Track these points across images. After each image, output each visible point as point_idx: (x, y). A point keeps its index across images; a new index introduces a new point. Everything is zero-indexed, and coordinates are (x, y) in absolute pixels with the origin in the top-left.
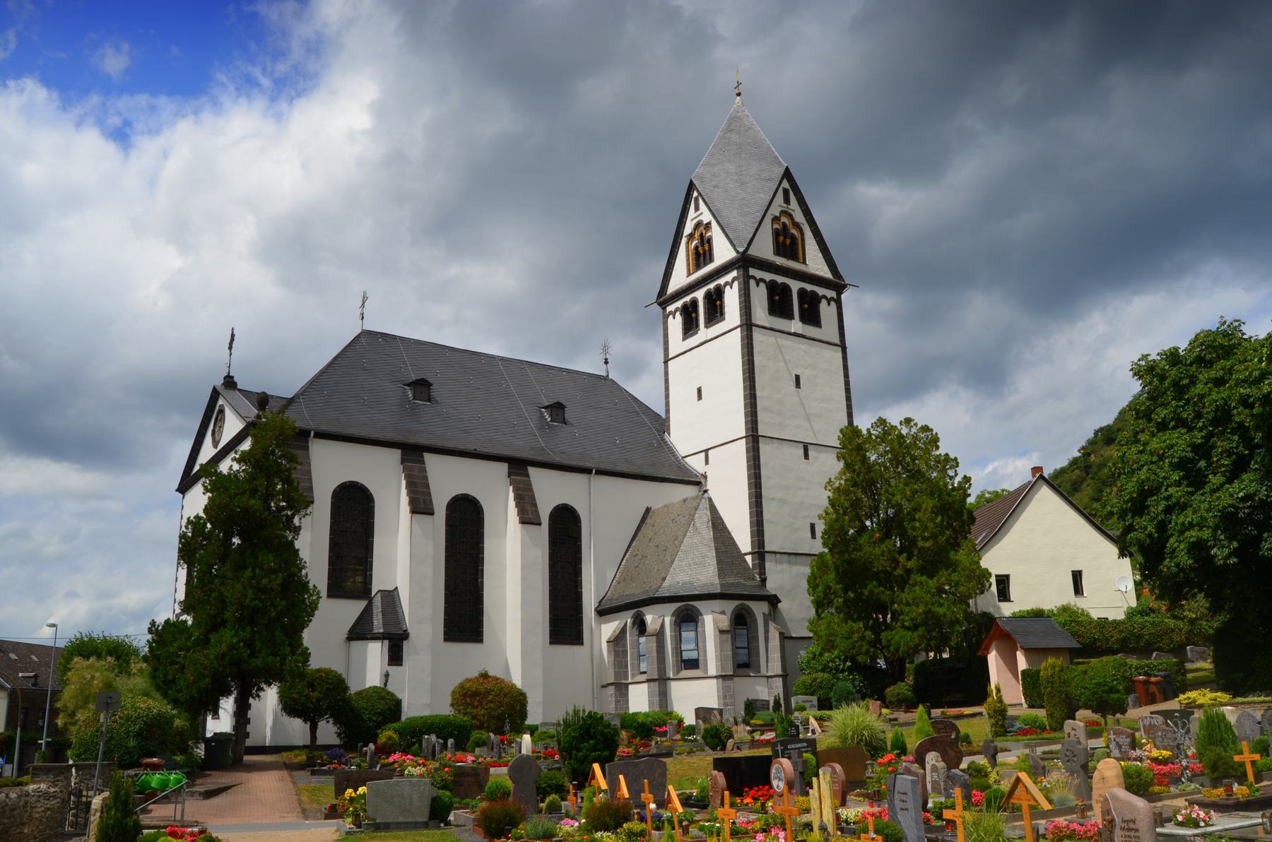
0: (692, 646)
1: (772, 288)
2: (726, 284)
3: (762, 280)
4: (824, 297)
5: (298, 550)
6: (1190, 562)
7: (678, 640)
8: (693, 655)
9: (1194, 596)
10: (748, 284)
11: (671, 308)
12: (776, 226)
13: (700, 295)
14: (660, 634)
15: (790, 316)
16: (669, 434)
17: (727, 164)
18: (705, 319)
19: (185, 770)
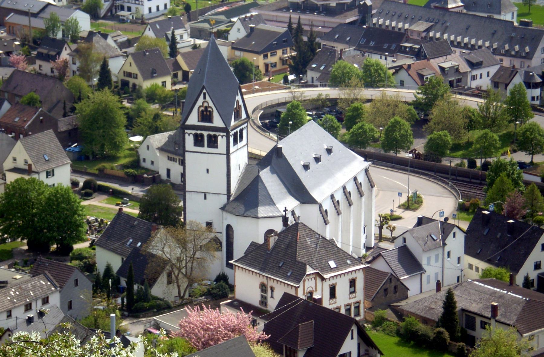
1: (196, 136)
12: (202, 108)
15: (203, 146)
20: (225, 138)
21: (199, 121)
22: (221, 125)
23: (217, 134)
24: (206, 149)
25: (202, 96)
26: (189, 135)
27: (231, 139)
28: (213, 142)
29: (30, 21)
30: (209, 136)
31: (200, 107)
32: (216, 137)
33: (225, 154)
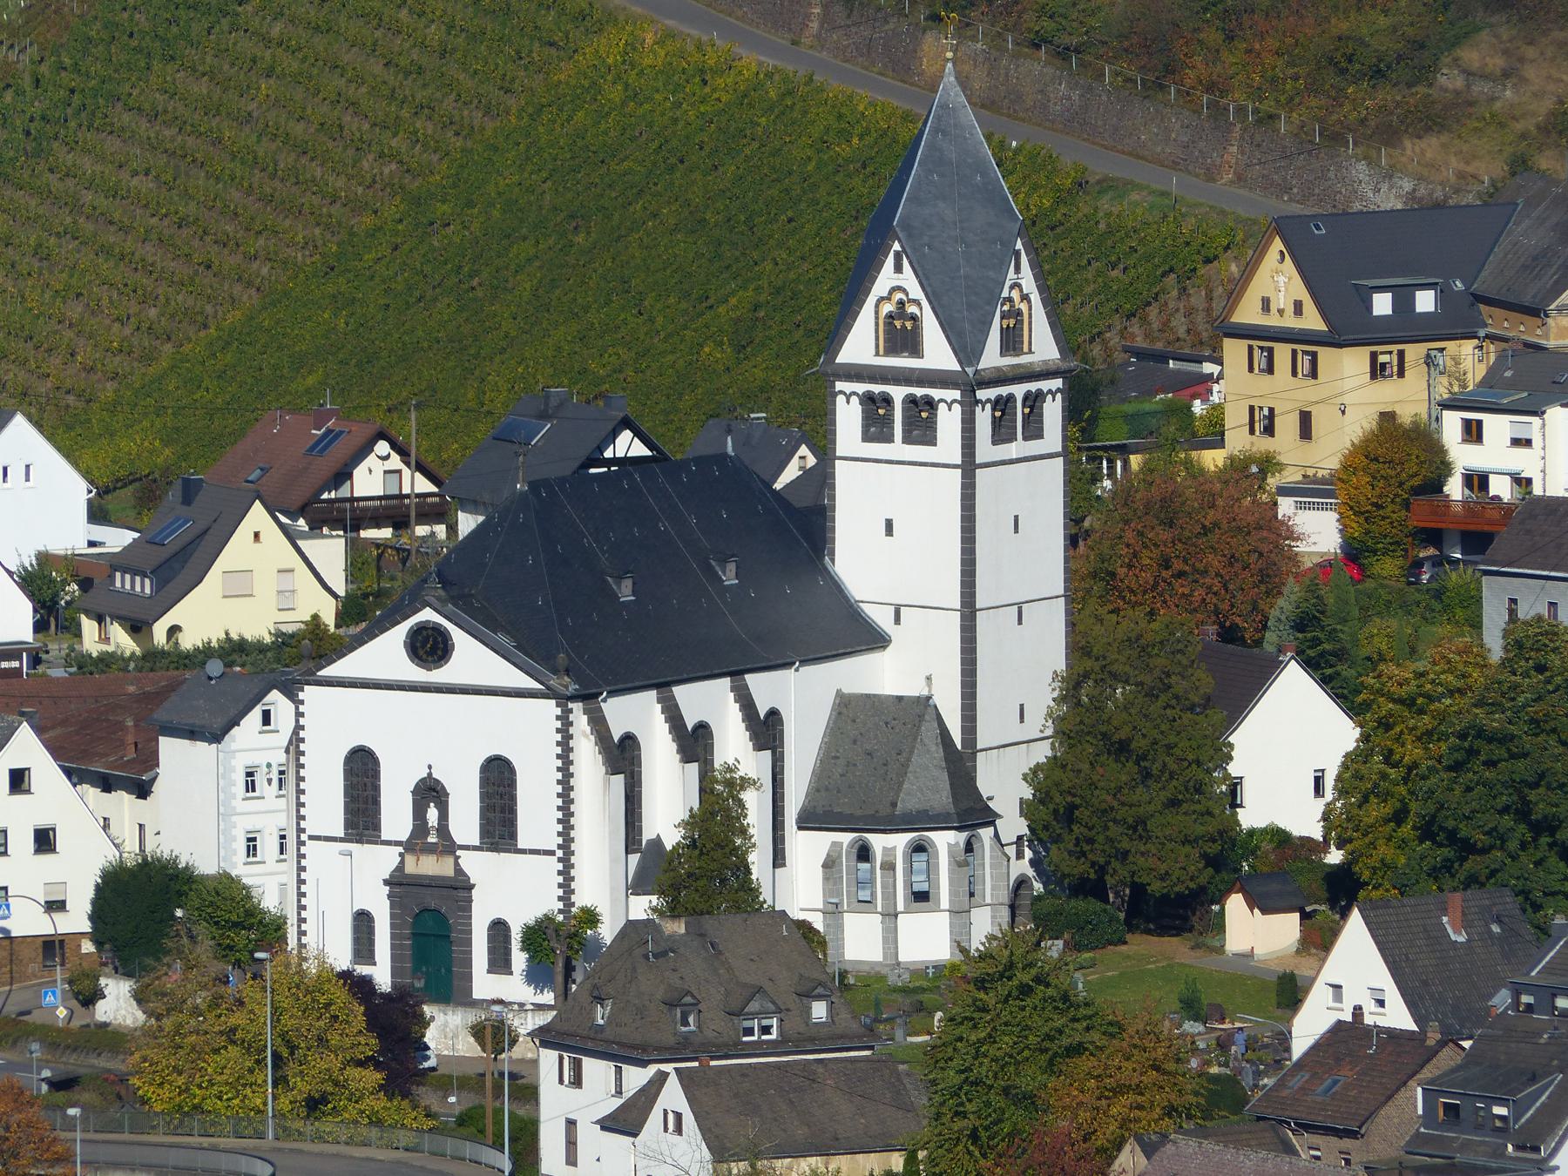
0: (923, 877)
1: (869, 400)
2: (1050, 391)
3: (854, 393)
4: (942, 400)
5: (239, 725)
6: (641, 907)
7: (909, 871)
8: (924, 887)
9: (420, 979)
10: (973, 413)
11: (982, 394)
12: (887, 308)
13: (1019, 390)
14: (889, 867)
15: (889, 439)
16: (833, 561)
17: (941, 204)
18: (904, 431)
19: (1236, 889)
20: (957, 408)
21: (877, 354)
22: (951, 364)
23: (936, 393)
24: (897, 448)
27: (984, 418)
28: (921, 425)
29: (523, 852)
30: (911, 401)
31: (881, 300)
32: (930, 404)
33: (955, 466)
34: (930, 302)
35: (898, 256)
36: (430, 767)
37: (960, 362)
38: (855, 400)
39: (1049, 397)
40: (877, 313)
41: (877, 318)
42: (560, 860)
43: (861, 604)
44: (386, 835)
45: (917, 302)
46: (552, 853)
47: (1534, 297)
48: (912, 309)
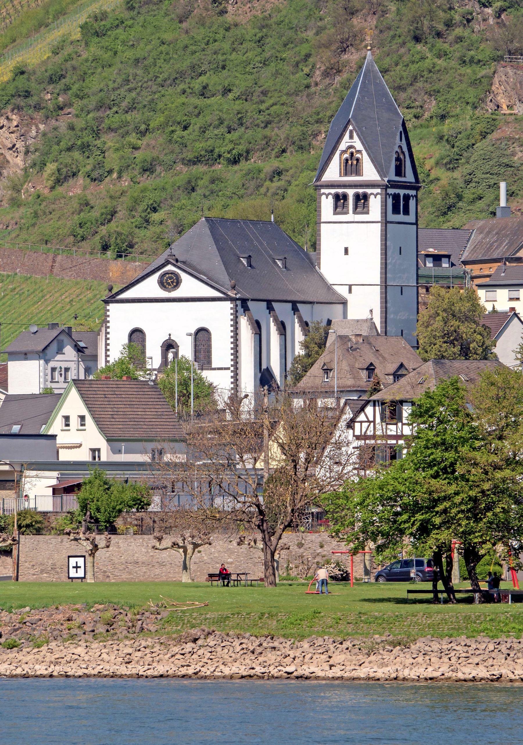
1: (337, 197)
3: (330, 194)
4: (372, 194)
12: (346, 156)
15: (347, 213)
16: (320, 268)
20: (379, 197)
21: (340, 176)
23: (369, 191)
24: (350, 216)
25: (347, 135)
26: (327, 196)
29: (215, 369)
31: (343, 152)
32: (366, 197)
34: (366, 150)
35: (351, 132)
36: (170, 335)
37: (381, 176)
38: (330, 197)
39: (232, 306)
40: (340, 158)
41: (340, 160)
42: (232, 371)
43: (334, 287)
44: (213, 366)
45: (359, 152)
46: (228, 369)
47: (498, 254)
48: (358, 155)
